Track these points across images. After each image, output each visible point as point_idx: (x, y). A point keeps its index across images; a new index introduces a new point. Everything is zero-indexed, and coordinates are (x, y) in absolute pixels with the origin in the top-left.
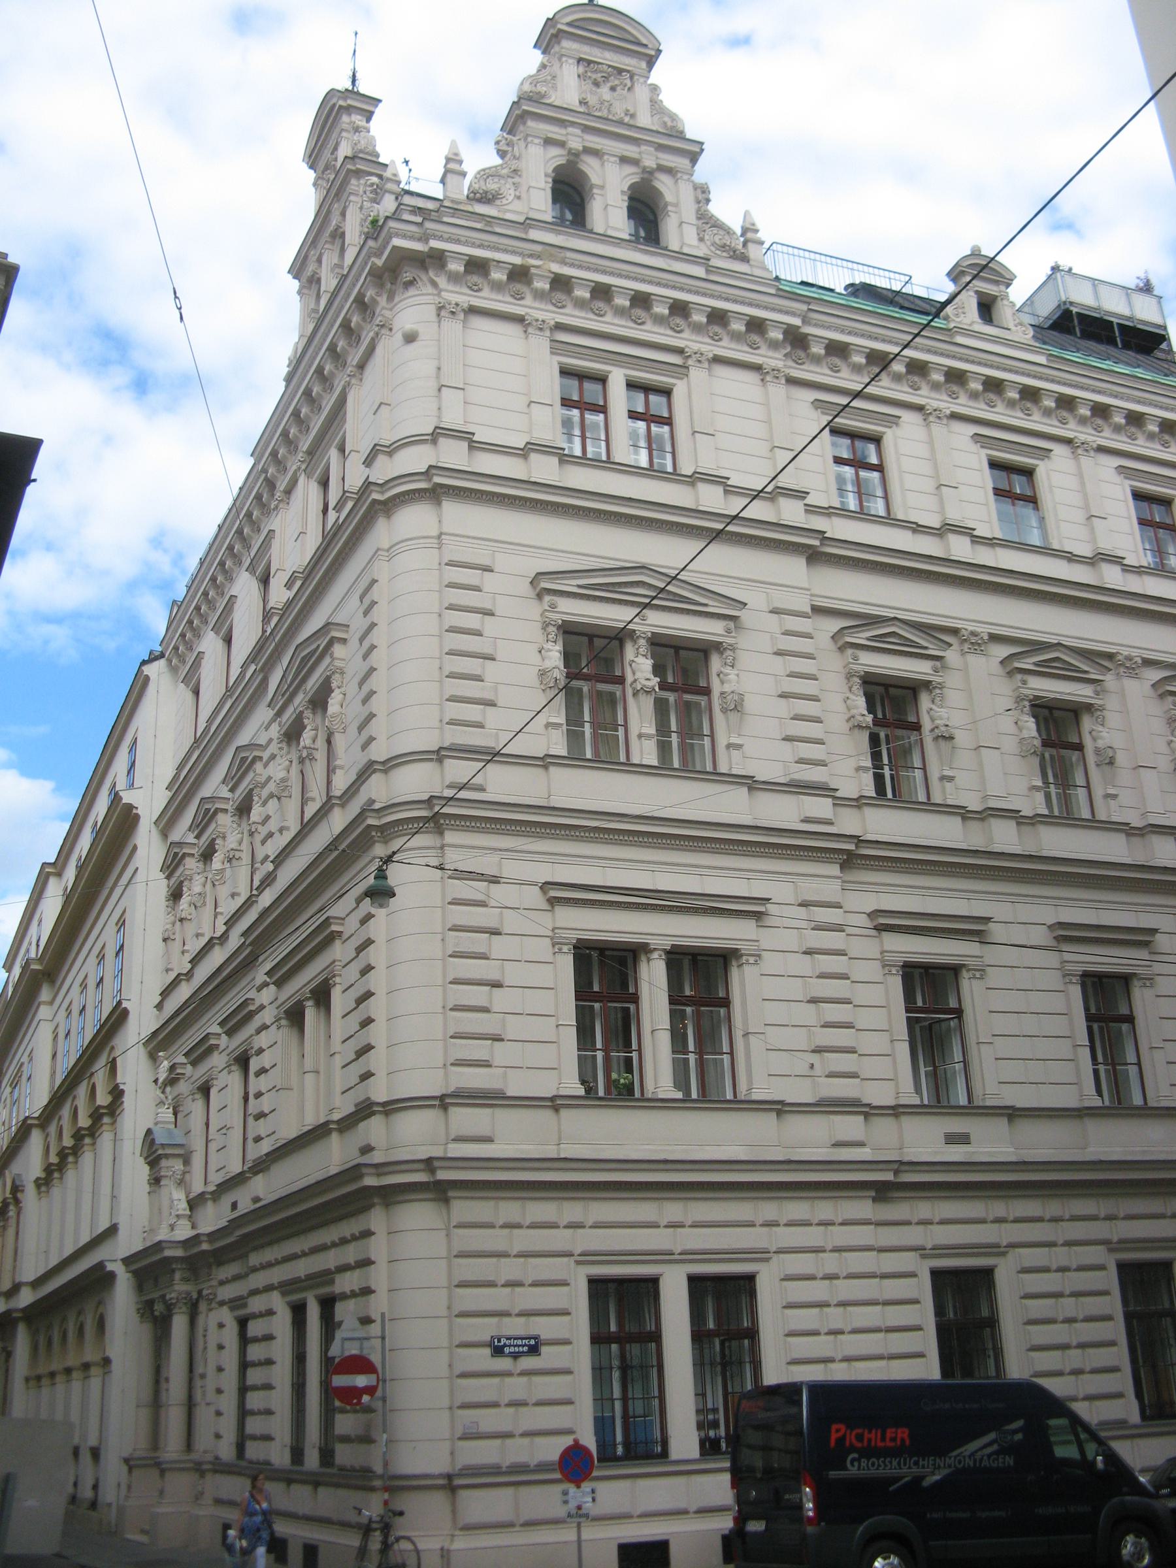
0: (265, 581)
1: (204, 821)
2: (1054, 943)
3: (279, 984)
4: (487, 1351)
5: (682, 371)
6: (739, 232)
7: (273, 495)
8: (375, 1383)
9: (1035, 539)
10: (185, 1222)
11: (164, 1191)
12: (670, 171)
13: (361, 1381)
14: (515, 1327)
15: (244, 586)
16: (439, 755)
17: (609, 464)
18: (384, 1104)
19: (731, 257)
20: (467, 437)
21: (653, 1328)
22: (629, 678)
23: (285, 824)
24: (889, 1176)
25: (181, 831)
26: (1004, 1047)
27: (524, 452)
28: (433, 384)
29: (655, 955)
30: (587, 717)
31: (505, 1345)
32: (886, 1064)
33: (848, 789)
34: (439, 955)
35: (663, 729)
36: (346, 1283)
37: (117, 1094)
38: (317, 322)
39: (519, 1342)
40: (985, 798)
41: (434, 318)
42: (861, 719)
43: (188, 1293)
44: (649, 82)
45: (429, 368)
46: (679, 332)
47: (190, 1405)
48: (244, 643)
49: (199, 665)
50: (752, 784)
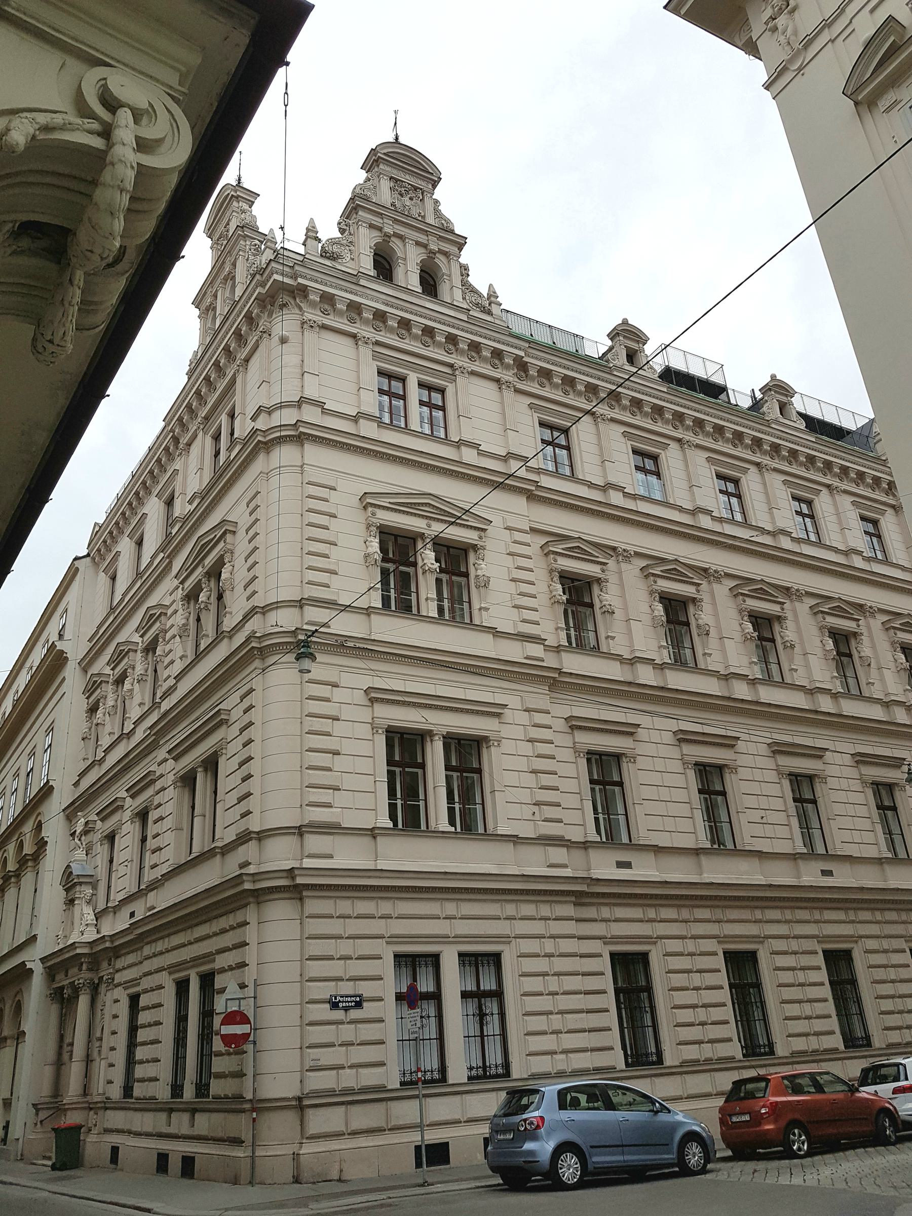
0: (170, 503)
1: (120, 656)
3: (176, 759)
4: (328, 1006)
5: (452, 377)
6: (486, 296)
7: (177, 448)
9: (658, 496)
11: (77, 909)
12: (446, 254)
14: (347, 988)
15: (153, 508)
17: (407, 430)
18: (258, 833)
20: (320, 405)
22: (420, 563)
24: (584, 888)
25: (101, 665)
26: (650, 807)
27: (355, 419)
28: (298, 370)
29: (437, 738)
30: (392, 586)
31: (340, 1001)
32: (578, 818)
33: (551, 641)
35: (440, 598)
37: (42, 844)
38: (211, 337)
39: (349, 999)
40: (633, 651)
41: (299, 329)
43: (92, 980)
44: (434, 197)
45: (296, 360)
47: (88, 1060)
48: (149, 548)
49: (117, 560)
50: (495, 633)
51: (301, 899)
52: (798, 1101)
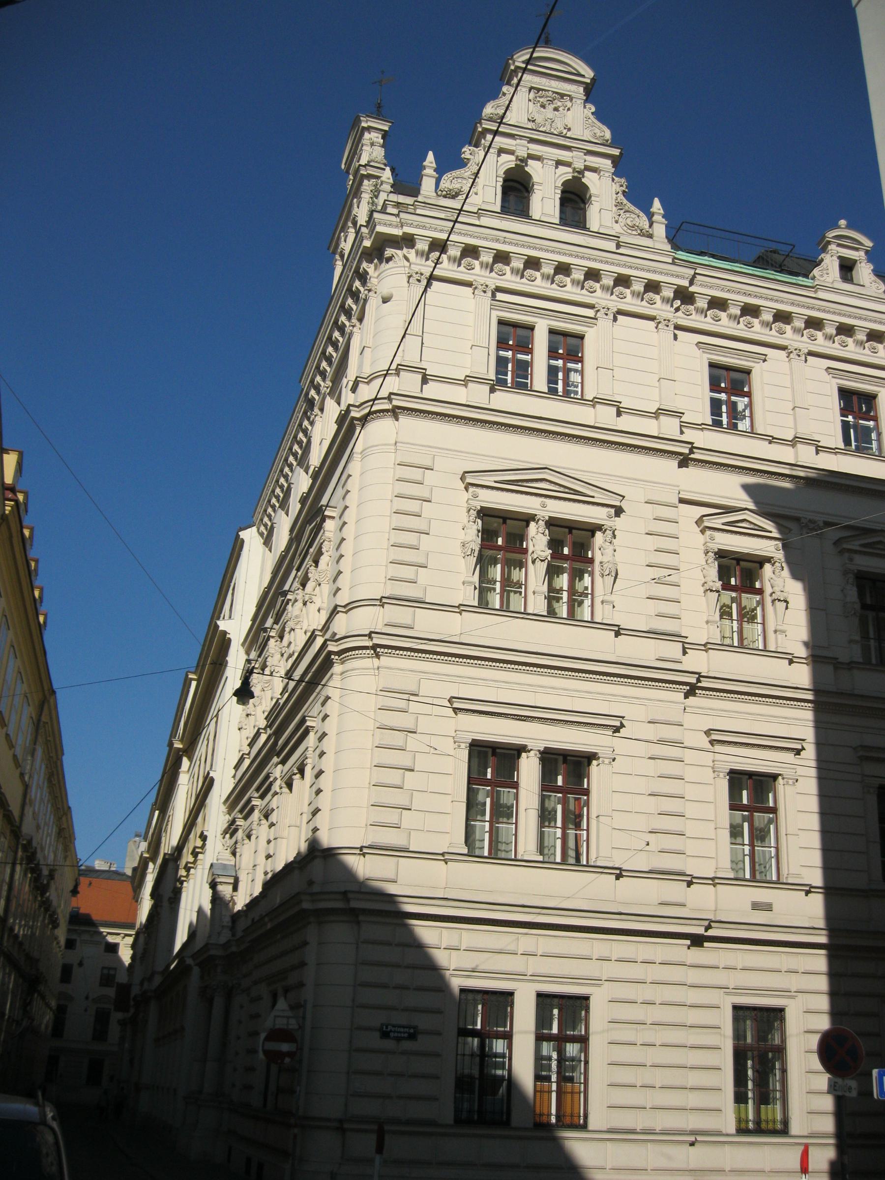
2: (709, 746)
4: (378, 1034)
8: (294, 1050)
13: (285, 1047)
16: (382, 602)
19: (639, 234)
21: (583, 1033)
22: (768, 590)
31: (391, 1031)
34: (369, 745)
39: (402, 1030)
42: (711, 584)
46: (592, 292)
51: (358, 923)
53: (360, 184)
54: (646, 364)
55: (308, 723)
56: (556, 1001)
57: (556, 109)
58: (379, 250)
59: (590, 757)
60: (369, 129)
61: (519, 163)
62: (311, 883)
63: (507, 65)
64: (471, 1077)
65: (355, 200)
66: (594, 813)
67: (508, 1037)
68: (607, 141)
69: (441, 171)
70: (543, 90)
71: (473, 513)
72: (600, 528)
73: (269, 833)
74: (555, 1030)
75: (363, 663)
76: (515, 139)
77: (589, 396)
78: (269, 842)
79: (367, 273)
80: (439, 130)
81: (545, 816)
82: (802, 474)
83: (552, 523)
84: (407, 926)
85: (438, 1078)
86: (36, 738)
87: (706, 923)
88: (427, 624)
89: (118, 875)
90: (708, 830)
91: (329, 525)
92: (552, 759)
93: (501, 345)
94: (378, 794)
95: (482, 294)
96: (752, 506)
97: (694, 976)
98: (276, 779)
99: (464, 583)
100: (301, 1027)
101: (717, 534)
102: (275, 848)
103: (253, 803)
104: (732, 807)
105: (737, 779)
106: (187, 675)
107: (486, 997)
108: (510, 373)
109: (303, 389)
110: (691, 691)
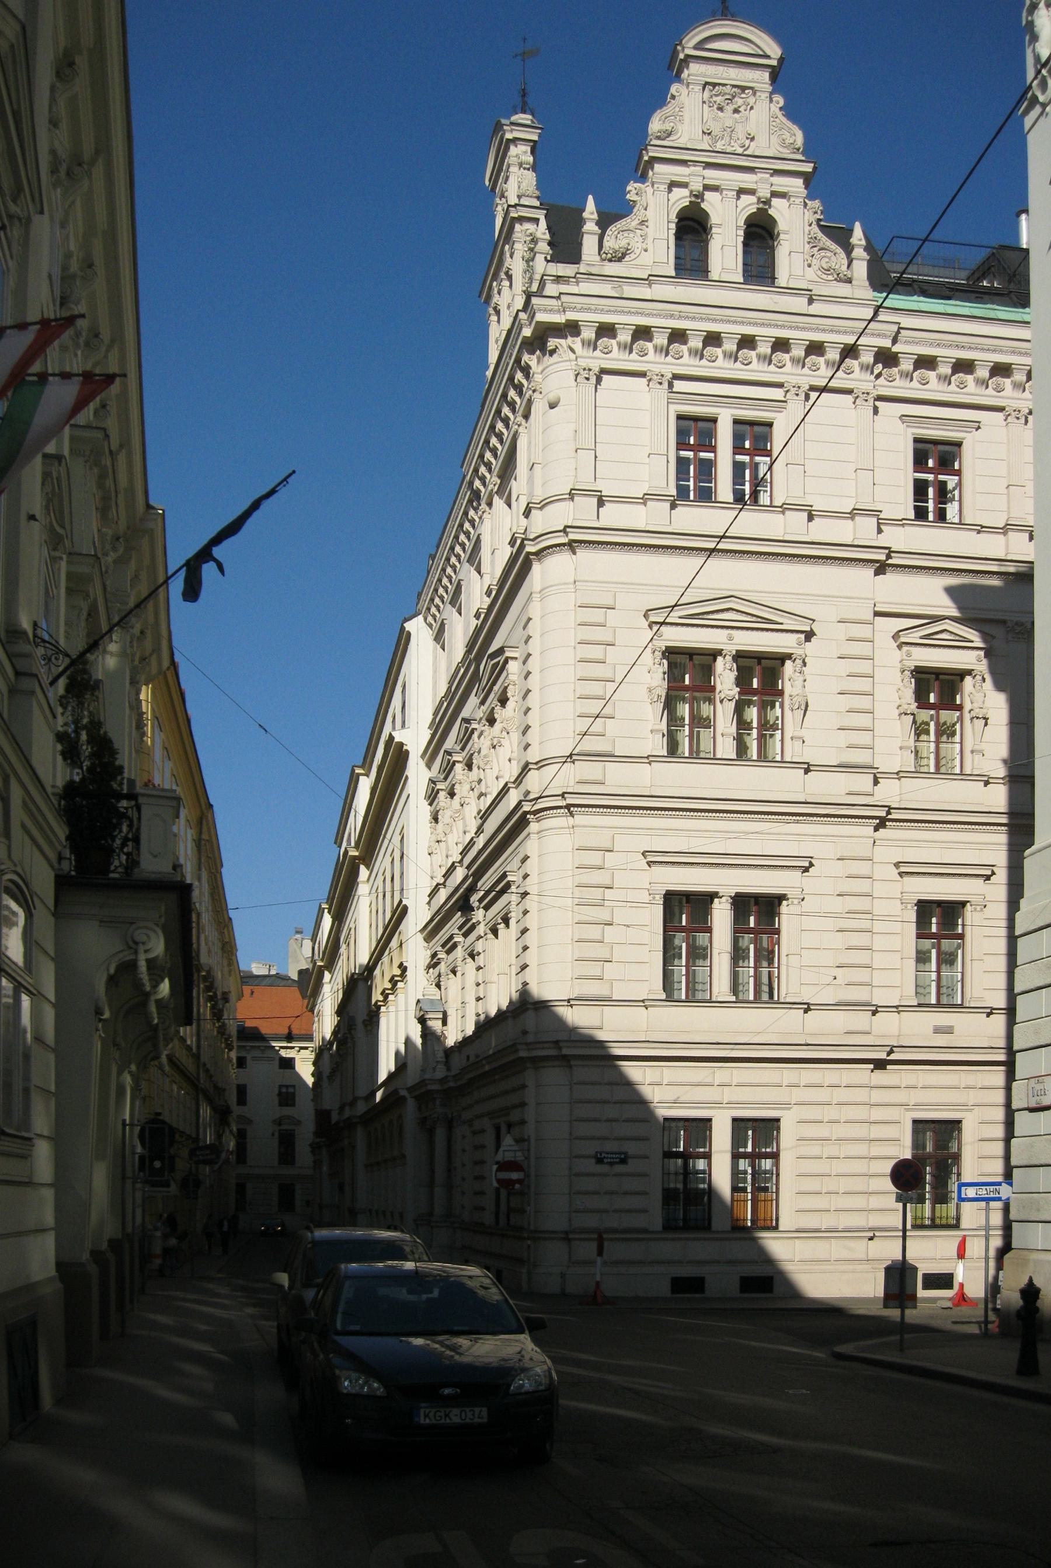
4: (593, 1161)
10: (440, 1066)
13: (514, 1176)
22: (967, 706)
23: (501, 773)
36: (515, 1116)
37: (403, 969)
46: (781, 367)
51: (571, 1067)
52: (794, 1353)
53: (511, 229)
54: (843, 455)
55: (509, 878)
56: (750, 1124)
57: (736, 111)
58: (541, 340)
59: (780, 899)
60: (515, 141)
61: (693, 199)
62: (525, 1033)
63: (675, 53)
64: (676, 1190)
65: (507, 247)
66: (784, 952)
67: (708, 1156)
68: (798, 150)
69: (605, 221)
70: (719, 84)
71: (658, 654)
72: (789, 656)
73: (477, 975)
74: (749, 1149)
75: (557, 821)
76: (688, 166)
77: (778, 502)
78: (478, 985)
79: (528, 367)
80: (596, 167)
81: (738, 955)
82: (1012, 570)
83: (740, 656)
84: (617, 1067)
85: (647, 1194)
86: (200, 859)
87: (888, 1049)
88: (619, 778)
89: (281, 979)
90: (894, 960)
91: (513, 667)
92: (742, 903)
93: (680, 447)
94: (579, 948)
95: (658, 386)
96: (955, 613)
97: (877, 1096)
98: (479, 923)
99: (652, 731)
100: (527, 1158)
101: (914, 650)
102: (485, 990)
103: (456, 939)
104: (919, 936)
105: (925, 909)
106: (353, 771)
107: (687, 1124)
108: (692, 480)
109: (464, 477)
110: (882, 823)
